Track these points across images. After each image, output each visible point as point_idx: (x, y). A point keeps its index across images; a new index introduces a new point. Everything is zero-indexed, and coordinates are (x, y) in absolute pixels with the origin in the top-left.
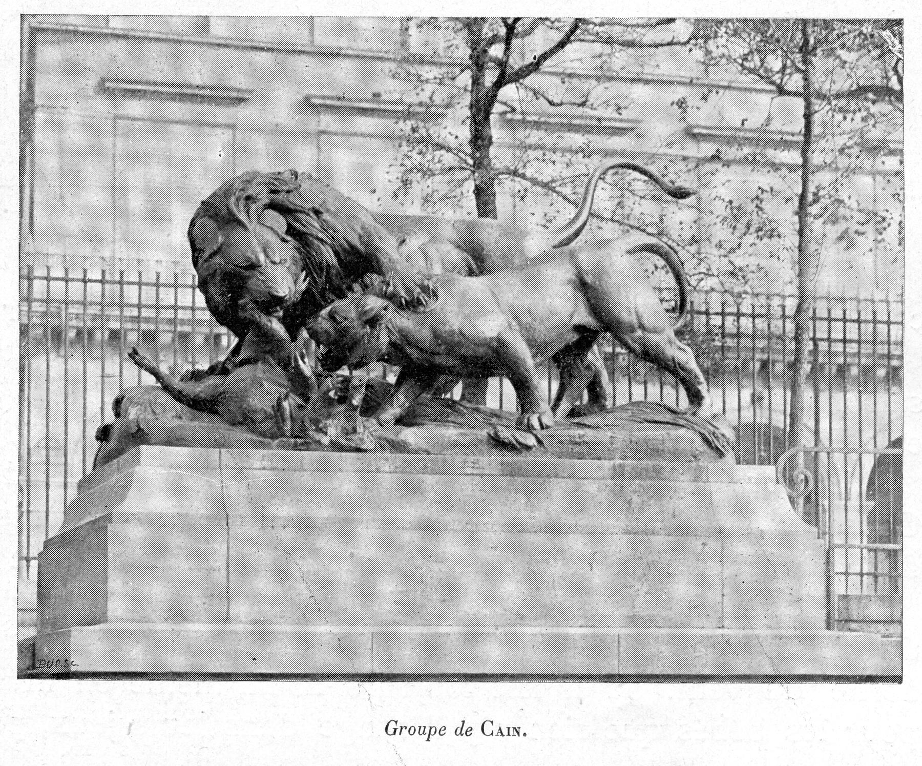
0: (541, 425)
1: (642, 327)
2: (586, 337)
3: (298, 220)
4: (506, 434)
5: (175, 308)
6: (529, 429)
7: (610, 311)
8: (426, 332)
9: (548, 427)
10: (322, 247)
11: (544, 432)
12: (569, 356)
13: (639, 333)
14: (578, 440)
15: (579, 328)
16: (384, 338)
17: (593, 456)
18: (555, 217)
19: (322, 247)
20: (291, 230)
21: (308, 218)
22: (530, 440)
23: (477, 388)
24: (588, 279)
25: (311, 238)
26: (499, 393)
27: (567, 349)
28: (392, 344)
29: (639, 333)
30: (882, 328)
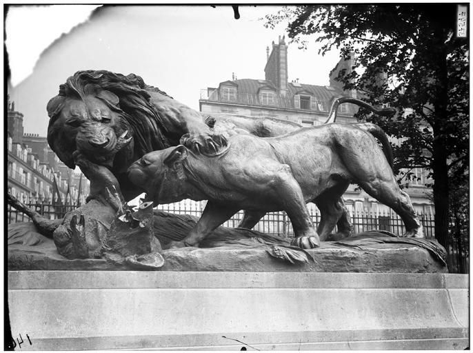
0: (310, 243)
1: (380, 178)
2: (339, 184)
3: (131, 100)
4: (283, 252)
5: (274, 215)
6: (301, 248)
7: (357, 164)
8: (217, 173)
9: (316, 246)
10: (147, 118)
11: (313, 250)
12: (329, 196)
13: (377, 181)
14: (339, 256)
15: (334, 177)
16: (181, 176)
17: (352, 269)
18: (258, 295)
19: (147, 118)
20: (121, 104)
21: (137, 99)
22: (302, 257)
23: (253, 217)
24: (342, 142)
25: (138, 112)
26: (271, 223)
27: (328, 191)
28: (188, 181)
29: (377, 181)
30: (276, 219)
